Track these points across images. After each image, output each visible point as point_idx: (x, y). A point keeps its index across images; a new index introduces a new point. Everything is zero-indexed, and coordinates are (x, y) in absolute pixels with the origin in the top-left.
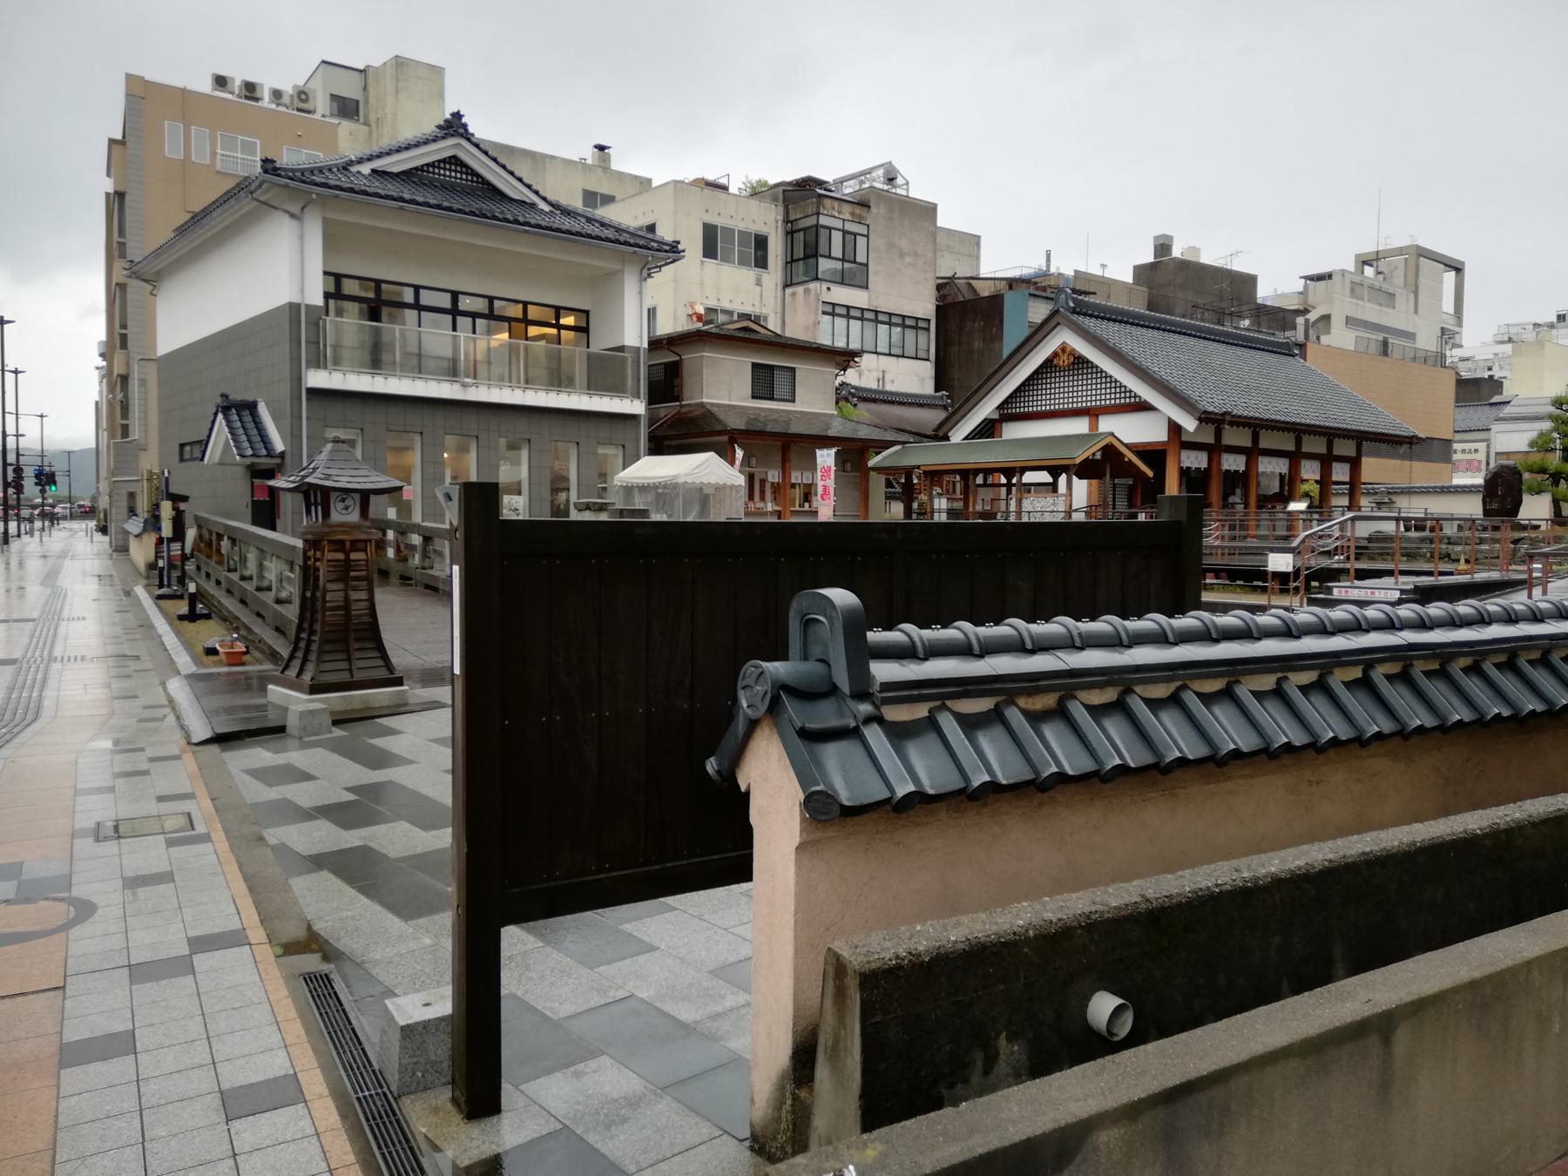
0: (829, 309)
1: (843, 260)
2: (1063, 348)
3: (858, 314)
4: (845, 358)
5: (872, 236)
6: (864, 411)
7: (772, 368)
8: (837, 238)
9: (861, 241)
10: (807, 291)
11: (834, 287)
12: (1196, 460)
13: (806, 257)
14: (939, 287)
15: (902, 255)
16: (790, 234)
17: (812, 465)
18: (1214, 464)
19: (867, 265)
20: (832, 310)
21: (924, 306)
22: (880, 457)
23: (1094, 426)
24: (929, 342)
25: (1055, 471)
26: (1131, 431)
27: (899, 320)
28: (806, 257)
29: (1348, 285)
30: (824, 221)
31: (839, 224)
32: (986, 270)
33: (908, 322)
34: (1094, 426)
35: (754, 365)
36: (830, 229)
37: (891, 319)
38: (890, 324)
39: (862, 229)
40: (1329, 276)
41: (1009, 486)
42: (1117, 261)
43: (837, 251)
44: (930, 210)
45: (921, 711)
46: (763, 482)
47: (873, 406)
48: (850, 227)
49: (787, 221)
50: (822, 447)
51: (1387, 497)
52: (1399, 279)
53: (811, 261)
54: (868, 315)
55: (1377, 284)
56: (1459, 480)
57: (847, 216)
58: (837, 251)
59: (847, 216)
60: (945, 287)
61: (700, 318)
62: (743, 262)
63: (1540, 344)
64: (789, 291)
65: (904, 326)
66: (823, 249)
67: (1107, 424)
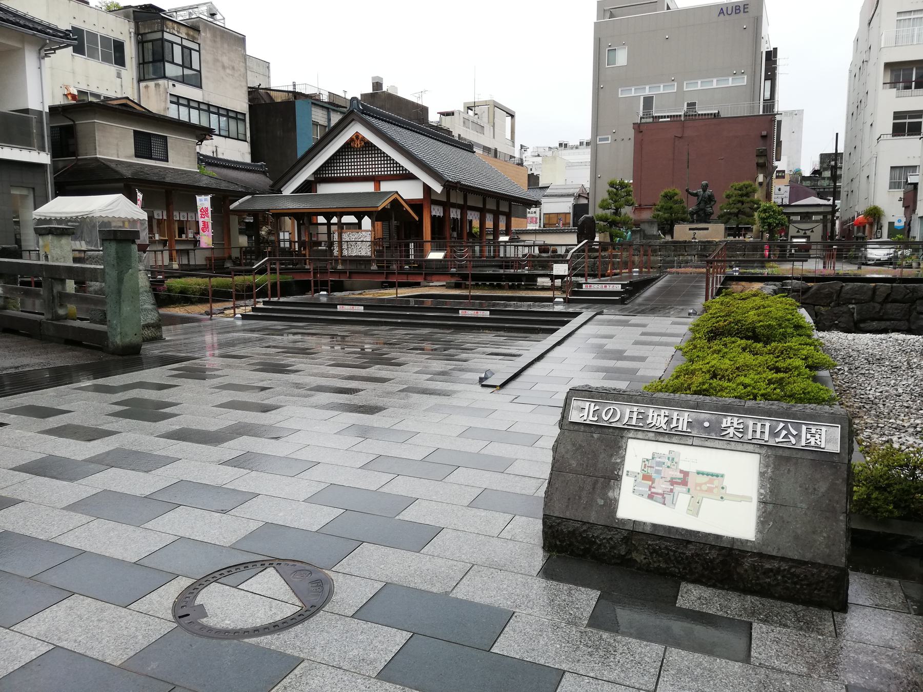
0: (175, 100)
1: (183, 66)
2: (357, 135)
4: (203, 133)
5: (202, 51)
6: (210, 171)
8: (177, 50)
9: (195, 55)
10: (157, 85)
11: (177, 84)
12: (437, 211)
13: (154, 62)
15: (224, 67)
17: (193, 207)
19: (200, 72)
20: (177, 100)
21: (241, 105)
23: (378, 187)
24: (246, 129)
25: (360, 216)
26: (409, 191)
28: (154, 62)
29: (462, 120)
30: (167, 36)
31: (178, 40)
32: (274, 85)
33: (231, 114)
34: (378, 187)
36: (172, 43)
37: (220, 111)
38: (219, 115)
40: (452, 114)
42: (355, 87)
43: (178, 59)
45: (656, 395)
47: (216, 169)
48: (186, 43)
49: (137, 33)
50: (200, 194)
52: (485, 119)
53: (159, 64)
54: (202, 106)
55: (475, 121)
56: (531, 227)
57: (184, 36)
58: (178, 59)
59: (184, 36)
60: (253, 93)
61: (74, 97)
62: (106, 59)
63: (554, 158)
64: (142, 84)
66: (168, 56)
67: (386, 187)
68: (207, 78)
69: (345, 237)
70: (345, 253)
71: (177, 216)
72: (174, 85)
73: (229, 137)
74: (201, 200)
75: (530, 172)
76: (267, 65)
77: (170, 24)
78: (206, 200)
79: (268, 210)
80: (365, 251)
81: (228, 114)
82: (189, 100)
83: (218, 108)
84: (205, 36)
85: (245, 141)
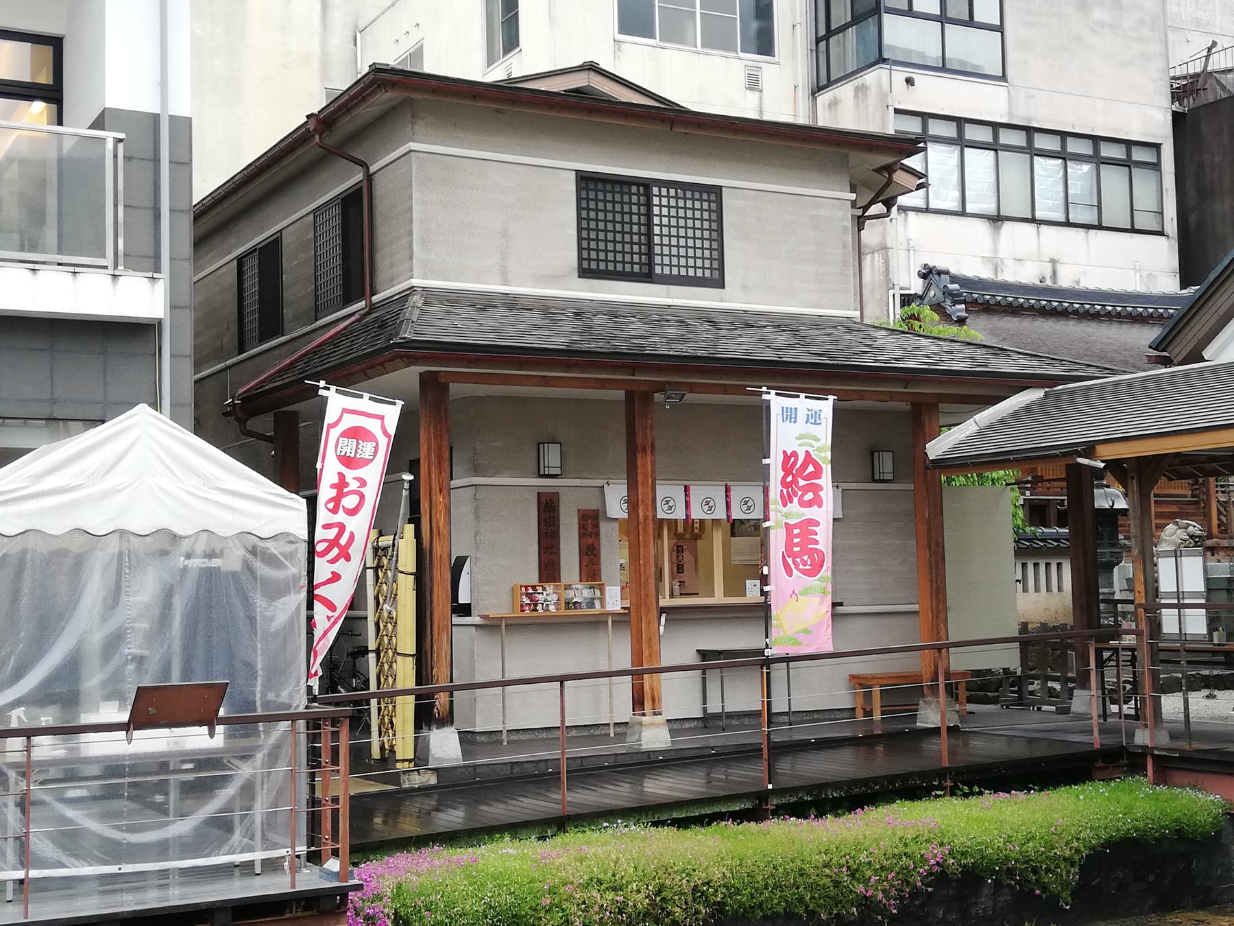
3: (985, 135)
7: (646, 185)
10: (861, 91)
13: (857, 19)
14: (1176, 96)
19: (1000, 29)
21: (1151, 120)
24: (1160, 194)
27: (1084, 148)
28: (857, 19)
33: (1107, 151)
35: (585, 180)
37: (1065, 145)
38: (1063, 156)
46: (590, 522)
51: (523, 858)
53: (871, 23)
54: (1006, 137)
62: (716, 40)
65: (1098, 160)
71: (670, 502)
72: (909, 81)
73: (1099, 227)
74: (814, 418)
75: (303, 859)
78: (814, 418)
79: (1089, 449)
81: (1099, 150)
82: (960, 122)
85: (1161, 233)
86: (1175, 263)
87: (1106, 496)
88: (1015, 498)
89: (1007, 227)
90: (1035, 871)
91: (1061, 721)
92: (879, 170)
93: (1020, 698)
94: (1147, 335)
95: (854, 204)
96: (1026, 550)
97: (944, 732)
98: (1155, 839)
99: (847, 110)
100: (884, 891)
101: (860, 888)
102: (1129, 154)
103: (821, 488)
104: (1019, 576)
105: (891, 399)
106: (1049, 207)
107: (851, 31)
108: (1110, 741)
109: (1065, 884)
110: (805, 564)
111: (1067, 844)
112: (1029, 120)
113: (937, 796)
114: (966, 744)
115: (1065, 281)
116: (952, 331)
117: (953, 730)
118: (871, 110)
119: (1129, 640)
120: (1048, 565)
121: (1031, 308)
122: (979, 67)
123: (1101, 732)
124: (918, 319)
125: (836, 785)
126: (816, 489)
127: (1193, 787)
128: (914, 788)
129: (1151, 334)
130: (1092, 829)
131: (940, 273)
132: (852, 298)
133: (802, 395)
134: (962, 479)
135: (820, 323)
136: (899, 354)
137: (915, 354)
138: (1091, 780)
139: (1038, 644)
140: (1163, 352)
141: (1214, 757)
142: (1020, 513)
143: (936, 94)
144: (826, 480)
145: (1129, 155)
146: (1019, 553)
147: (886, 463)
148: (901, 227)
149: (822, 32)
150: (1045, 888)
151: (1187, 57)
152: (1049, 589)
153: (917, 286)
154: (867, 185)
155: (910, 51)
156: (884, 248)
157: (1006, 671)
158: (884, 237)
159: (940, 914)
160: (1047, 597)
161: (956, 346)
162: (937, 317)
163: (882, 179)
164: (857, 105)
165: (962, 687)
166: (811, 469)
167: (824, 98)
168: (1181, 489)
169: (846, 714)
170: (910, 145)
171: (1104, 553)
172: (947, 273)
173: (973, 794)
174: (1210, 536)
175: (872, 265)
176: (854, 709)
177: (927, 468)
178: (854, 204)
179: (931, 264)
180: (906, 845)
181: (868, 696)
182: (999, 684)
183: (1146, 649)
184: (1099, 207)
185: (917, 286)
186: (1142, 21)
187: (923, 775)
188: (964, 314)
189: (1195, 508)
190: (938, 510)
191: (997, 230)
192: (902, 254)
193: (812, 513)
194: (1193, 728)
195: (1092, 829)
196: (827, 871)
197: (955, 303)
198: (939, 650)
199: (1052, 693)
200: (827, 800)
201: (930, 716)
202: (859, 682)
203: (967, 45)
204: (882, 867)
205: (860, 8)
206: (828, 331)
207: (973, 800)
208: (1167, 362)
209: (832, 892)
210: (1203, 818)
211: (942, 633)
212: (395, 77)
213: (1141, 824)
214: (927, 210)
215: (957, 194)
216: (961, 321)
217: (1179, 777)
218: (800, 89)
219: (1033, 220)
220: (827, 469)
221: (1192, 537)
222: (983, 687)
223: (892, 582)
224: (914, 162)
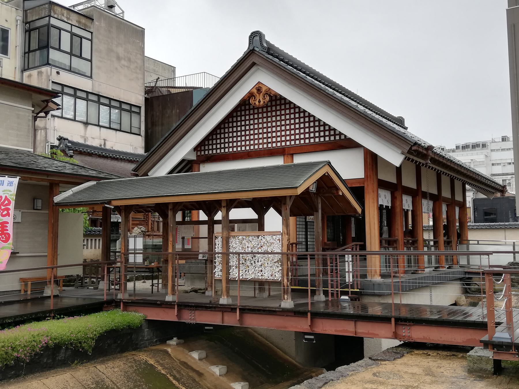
1: (71, 54)
2: (259, 88)
3: (84, 95)
5: (94, 40)
8: (66, 37)
9: (86, 44)
10: (40, 73)
13: (40, 48)
14: (146, 92)
15: (119, 58)
16: (28, 32)
18: (398, 203)
19: (91, 61)
21: (138, 98)
22: (69, 193)
24: (140, 122)
30: (53, 21)
31: (68, 27)
32: (179, 83)
33: (124, 106)
37: (111, 102)
38: (110, 106)
39: (89, 36)
41: (211, 223)
43: (66, 45)
44: (138, 33)
48: (75, 30)
49: (26, 22)
53: (45, 50)
54: (91, 97)
58: (66, 45)
65: (121, 109)
66: (53, 42)
68: (99, 68)
69: (235, 245)
70: (234, 274)
72: (58, 73)
73: (120, 130)
76: (173, 69)
77: (59, 9)
78: (11, 184)
79: (109, 202)
80: (271, 271)
81: (122, 106)
82: (75, 89)
83: (110, 99)
84: (98, 25)
85: (140, 135)
86: (143, 145)
87: (116, 217)
88: (86, 217)
89: (90, 127)
90: (80, 343)
91: (95, 292)
92: (43, 101)
93: (82, 284)
94: (133, 166)
95: (33, 112)
96: (88, 235)
97: (52, 297)
98: (121, 329)
99: (34, 79)
100: (25, 354)
101: (15, 354)
102: (131, 108)
103: (9, 209)
104: (85, 243)
105: (42, 181)
106: (104, 122)
107: (38, 52)
108: (109, 298)
109: (90, 346)
110: (3, 238)
111: (92, 333)
112: (99, 92)
113: (48, 320)
114: (61, 301)
115: (108, 147)
116: (67, 159)
117: (56, 297)
118: (43, 80)
119: (119, 264)
120: (95, 240)
121: (96, 154)
122: (85, 73)
123: (107, 295)
124: (56, 154)
125: (10, 318)
126: (8, 210)
127: (135, 312)
128: (39, 317)
129: (133, 166)
130: (101, 327)
131: (65, 139)
132: (31, 144)
133: (7, 176)
134: (68, 210)
135: (17, 152)
136: (46, 165)
137: (54, 166)
138: (102, 311)
139: (91, 268)
140: (136, 173)
141: (142, 301)
142: (88, 222)
143: (66, 78)
144: (12, 207)
145: (128, 108)
146: (85, 236)
147: (39, 203)
148: (52, 122)
149: (27, 50)
150: (83, 348)
151: (150, 80)
152: (95, 248)
153: (57, 143)
154: (39, 106)
155: (61, 63)
156: (45, 129)
157: (78, 275)
158: (46, 125)
159: (45, 360)
160: (93, 251)
161: (67, 165)
162: (62, 154)
163: (44, 105)
164: (38, 78)
165: (61, 281)
166: (6, 202)
167: (26, 74)
168: (141, 216)
169: (18, 292)
170: (55, 94)
171: (113, 236)
172: (67, 139)
173: (61, 318)
174: (148, 231)
175: (40, 135)
176: (20, 290)
177: (53, 206)
178: (33, 112)
179: (62, 136)
180: (34, 337)
181: (26, 285)
182: (75, 280)
183: (123, 267)
184: (120, 124)
185: (57, 143)
186: (137, 67)
187: (44, 312)
188: (72, 154)
189: (145, 222)
190: (57, 220)
191: (86, 128)
192: (52, 131)
193: (5, 219)
194: (136, 292)
195: (101, 327)
196: (3, 349)
197: (69, 150)
198: (53, 269)
199: (93, 282)
200: (6, 323)
201: (48, 292)
202: (23, 281)
203: (77, 63)
204: (25, 346)
205: (41, 45)
206: (20, 155)
207: (61, 320)
208: (137, 175)
209: (5, 356)
210: (137, 321)
211: (55, 263)
212: (149, 120)
213: (117, 325)
214: (62, 117)
215: (73, 113)
216: (71, 156)
217: (131, 308)
218: (17, 68)
219: (98, 125)
220: (13, 203)
221: (142, 231)
222: (69, 281)
223: (37, 245)
224: (57, 100)
